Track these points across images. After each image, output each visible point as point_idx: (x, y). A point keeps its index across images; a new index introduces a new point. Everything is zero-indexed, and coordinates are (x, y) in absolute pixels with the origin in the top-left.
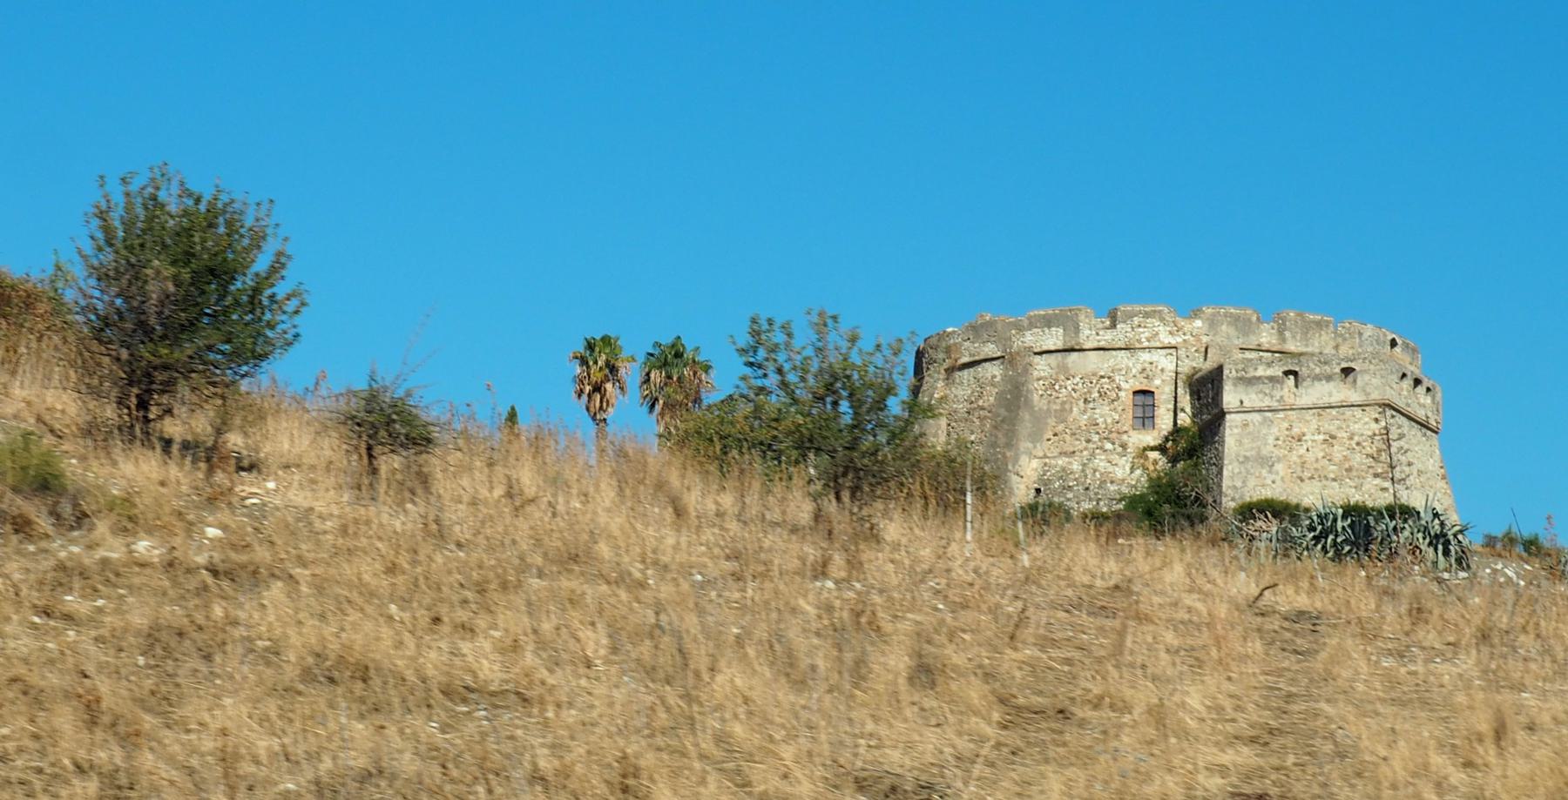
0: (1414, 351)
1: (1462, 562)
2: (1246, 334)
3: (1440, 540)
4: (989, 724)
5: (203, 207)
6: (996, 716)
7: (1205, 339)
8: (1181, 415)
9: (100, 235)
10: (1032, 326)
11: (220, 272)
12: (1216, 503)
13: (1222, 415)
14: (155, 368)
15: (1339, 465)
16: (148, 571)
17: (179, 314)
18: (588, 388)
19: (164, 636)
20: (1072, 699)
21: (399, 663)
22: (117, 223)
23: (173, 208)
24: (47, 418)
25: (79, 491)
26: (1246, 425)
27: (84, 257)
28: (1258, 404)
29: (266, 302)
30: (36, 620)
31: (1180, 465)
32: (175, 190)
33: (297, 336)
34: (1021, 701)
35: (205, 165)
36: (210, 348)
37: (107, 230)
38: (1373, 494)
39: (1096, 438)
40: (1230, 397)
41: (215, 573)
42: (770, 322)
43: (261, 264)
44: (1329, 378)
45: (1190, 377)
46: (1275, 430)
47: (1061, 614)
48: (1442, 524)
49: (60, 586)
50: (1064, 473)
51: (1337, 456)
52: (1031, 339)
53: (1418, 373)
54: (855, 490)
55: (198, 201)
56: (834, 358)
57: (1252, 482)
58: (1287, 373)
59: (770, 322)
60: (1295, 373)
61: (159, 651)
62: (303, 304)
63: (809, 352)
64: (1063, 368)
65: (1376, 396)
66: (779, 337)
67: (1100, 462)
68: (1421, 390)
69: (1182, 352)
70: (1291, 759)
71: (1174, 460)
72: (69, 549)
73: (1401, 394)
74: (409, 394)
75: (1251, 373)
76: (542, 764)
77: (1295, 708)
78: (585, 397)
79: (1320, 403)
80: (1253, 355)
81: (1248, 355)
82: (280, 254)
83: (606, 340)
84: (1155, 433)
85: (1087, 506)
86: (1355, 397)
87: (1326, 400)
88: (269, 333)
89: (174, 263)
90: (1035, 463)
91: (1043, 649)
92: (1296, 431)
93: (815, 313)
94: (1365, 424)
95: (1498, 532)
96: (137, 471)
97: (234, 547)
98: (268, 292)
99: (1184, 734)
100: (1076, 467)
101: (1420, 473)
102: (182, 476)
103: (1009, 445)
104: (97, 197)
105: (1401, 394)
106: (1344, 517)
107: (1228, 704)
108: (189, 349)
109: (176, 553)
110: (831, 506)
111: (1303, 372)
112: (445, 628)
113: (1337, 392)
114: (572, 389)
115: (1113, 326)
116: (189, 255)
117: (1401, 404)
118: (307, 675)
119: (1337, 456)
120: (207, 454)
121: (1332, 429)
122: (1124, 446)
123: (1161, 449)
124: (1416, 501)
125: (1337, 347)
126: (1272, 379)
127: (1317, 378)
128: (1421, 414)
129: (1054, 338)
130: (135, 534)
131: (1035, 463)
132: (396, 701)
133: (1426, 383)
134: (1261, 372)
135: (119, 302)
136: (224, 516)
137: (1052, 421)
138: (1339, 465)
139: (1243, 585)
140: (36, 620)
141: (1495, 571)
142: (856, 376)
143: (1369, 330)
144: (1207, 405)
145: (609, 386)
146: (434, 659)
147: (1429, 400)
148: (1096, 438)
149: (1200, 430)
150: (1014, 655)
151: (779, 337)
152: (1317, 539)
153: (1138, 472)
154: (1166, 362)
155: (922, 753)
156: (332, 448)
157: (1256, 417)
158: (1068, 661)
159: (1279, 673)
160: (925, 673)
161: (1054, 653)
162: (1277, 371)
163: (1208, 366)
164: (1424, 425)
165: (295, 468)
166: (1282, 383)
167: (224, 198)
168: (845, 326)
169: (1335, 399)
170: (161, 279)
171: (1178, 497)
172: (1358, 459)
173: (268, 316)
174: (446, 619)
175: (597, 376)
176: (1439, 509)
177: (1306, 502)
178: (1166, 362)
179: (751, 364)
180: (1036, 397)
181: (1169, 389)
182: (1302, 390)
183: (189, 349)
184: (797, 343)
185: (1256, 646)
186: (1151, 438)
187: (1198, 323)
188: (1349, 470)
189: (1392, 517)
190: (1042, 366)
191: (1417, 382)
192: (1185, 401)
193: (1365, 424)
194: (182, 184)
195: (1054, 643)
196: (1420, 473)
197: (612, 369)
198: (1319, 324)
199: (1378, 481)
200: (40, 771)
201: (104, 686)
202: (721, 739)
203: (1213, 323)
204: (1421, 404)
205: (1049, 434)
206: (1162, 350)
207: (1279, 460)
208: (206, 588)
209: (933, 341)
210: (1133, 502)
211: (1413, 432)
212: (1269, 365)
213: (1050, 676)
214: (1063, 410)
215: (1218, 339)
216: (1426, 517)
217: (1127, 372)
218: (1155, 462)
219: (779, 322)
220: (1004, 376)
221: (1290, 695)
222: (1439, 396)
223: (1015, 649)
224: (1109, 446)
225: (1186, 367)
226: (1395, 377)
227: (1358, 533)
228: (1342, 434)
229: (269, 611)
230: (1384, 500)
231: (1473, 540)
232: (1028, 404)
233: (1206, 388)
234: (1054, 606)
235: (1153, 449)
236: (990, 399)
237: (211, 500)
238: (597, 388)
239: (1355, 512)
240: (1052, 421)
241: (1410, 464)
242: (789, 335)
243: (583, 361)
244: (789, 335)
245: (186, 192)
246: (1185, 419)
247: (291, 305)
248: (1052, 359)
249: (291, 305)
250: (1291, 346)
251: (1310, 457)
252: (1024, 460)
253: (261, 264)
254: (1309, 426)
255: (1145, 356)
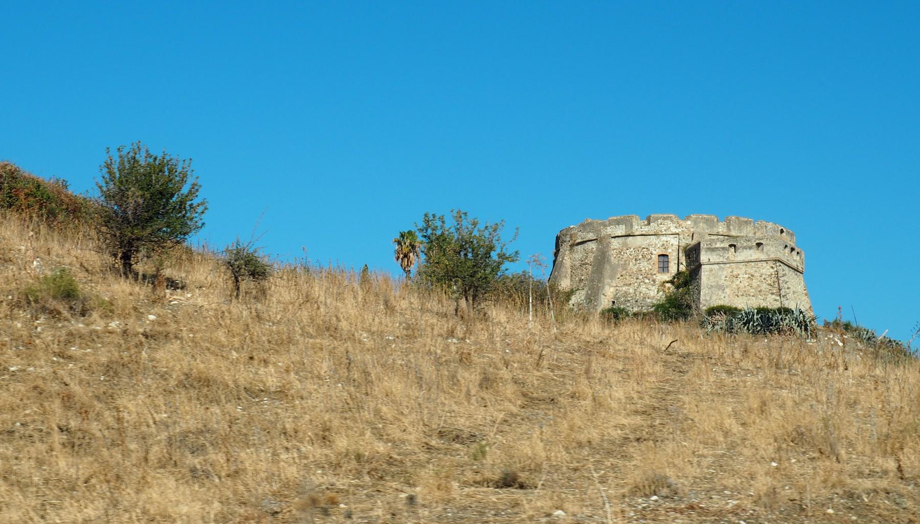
0: (792, 235)
1: (814, 334)
2: (712, 227)
3: (804, 325)
4: (515, 406)
5: (157, 163)
6: (519, 402)
7: (692, 230)
8: (681, 266)
9: (107, 176)
10: (610, 224)
11: (165, 194)
12: (697, 308)
13: (700, 266)
14: (133, 240)
15: (755, 289)
16: (113, 336)
17: (145, 215)
18: (401, 256)
19: (115, 366)
20: (560, 394)
21: (226, 378)
22: (116, 170)
23: (142, 163)
24: (86, 265)
25: (84, 298)
26: (711, 270)
27: (100, 187)
28: (717, 261)
29: (188, 208)
30: (55, 359)
31: (680, 290)
32: (143, 154)
33: (203, 224)
34: (535, 395)
35: (158, 142)
36: (159, 230)
37: (111, 173)
38: (771, 302)
39: (641, 277)
40: (704, 257)
41: (146, 337)
42: (434, 216)
43: (185, 190)
44: (750, 248)
45: (685, 248)
46: (725, 273)
47: (568, 355)
48: (804, 316)
49: (68, 343)
50: (626, 294)
51: (755, 285)
52: (610, 230)
53: (793, 245)
54: (475, 297)
55: (155, 159)
56: (465, 233)
57: (714, 298)
58: (731, 246)
59: (434, 216)
60: (735, 246)
61: (112, 373)
62: (206, 209)
63: (453, 230)
64: (625, 244)
65: (773, 256)
66: (439, 224)
67: (643, 289)
68: (794, 253)
69: (681, 236)
70: (658, 422)
71: (678, 287)
72: (79, 326)
73: (785, 255)
74: (255, 252)
75: (714, 246)
76: (287, 426)
77: (669, 398)
78: (400, 260)
79: (747, 259)
80: (715, 237)
81: (712, 237)
82: (194, 185)
83: (410, 233)
84: (669, 275)
85: (636, 310)
86: (763, 257)
87: (749, 258)
88: (189, 223)
89: (142, 189)
90: (612, 289)
91: (552, 371)
92: (735, 273)
93: (455, 212)
94: (767, 269)
95: (831, 320)
96: (122, 289)
97: (159, 324)
98: (189, 203)
99: (609, 410)
100: (631, 291)
101: (794, 293)
102: (142, 291)
103: (599, 281)
104: (105, 158)
105: (785, 255)
106: (758, 314)
107: (635, 396)
108: (149, 230)
109: (128, 327)
110: (463, 303)
111: (738, 245)
112: (256, 362)
113: (754, 254)
114: (394, 256)
115: (649, 224)
116: (150, 185)
117: (785, 260)
118: (181, 384)
119: (755, 285)
120: (154, 279)
121: (752, 272)
122: (654, 281)
123: (672, 282)
124: (792, 306)
125: (755, 233)
126: (723, 248)
127: (745, 248)
128: (794, 264)
129: (621, 230)
130: (112, 318)
131: (612, 289)
132: (223, 397)
133: (797, 250)
134: (718, 246)
135: (116, 207)
136: (157, 309)
137: (620, 269)
138: (755, 289)
139: (666, 341)
140: (55, 359)
141: (829, 339)
142: (475, 242)
143: (770, 225)
144: (693, 261)
145: (411, 255)
146: (244, 376)
147: (798, 258)
148: (641, 277)
149: (690, 273)
150: (539, 374)
151: (439, 224)
152: (745, 324)
153: (661, 293)
154: (674, 241)
155: (476, 419)
156: (222, 279)
157: (716, 267)
158: (563, 376)
159: (667, 381)
160: (487, 382)
161: (557, 372)
162: (726, 245)
163: (694, 242)
164: (796, 270)
165: (202, 290)
166: (728, 250)
167: (167, 158)
168: (470, 218)
169: (754, 257)
170: (135, 196)
171: (678, 306)
172: (764, 286)
173: (188, 214)
174: (256, 357)
175: (405, 250)
176: (803, 309)
177: (740, 307)
178: (674, 241)
179: (425, 236)
180: (612, 258)
181: (675, 254)
182: (738, 254)
183: (149, 230)
184: (447, 226)
185: (658, 368)
186: (667, 277)
187: (689, 222)
188: (760, 291)
189: (780, 313)
190: (615, 243)
191: (793, 249)
192: (683, 259)
193: (767, 269)
194: (147, 151)
195: (559, 368)
196: (794, 293)
197: (413, 247)
198: (746, 222)
199: (773, 296)
200: (41, 431)
201: (75, 388)
202: (377, 412)
203: (696, 223)
204: (795, 260)
205: (619, 276)
206: (671, 236)
207: (727, 287)
208: (141, 343)
209: (564, 232)
210: (658, 307)
211: (791, 273)
212: (722, 242)
213: (553, 383)
214: (625, 264)
215: (698, 230)
216: (796, 313)
217: (656, 246)
218: (669, 288)
219: (438, 216)
220: (597, 248)
221: (669, 392)
222: (803, 256)
223: (538, 370)
224: (647, 281)
225: (683, 243)
226: (782, 247)
227: (766, 322)
228: (757, 274)
229: (169, 356)
230: (776, 305)
231: (819, 324)
232: (609, 261)
233: (692, 253)
234: (566, 351)
235: (668, 282)
236: (591, 259)
237: (154, 302)
238: (406, 256)
239: (762, 311)
240: (620, 269)
241: (788, 288)
242: (443, 222)
243: (399, 243)
244: (443, 222)
245: (149, 155)
246: (683, 268)
247: (200, 209)
248: (620, 240)
249: (200, 209)
250: (733, 233)
251: (742, 285)
252: (607, 287)
253: (185, 190)
254: (741, 270)
255: (664, 238)
